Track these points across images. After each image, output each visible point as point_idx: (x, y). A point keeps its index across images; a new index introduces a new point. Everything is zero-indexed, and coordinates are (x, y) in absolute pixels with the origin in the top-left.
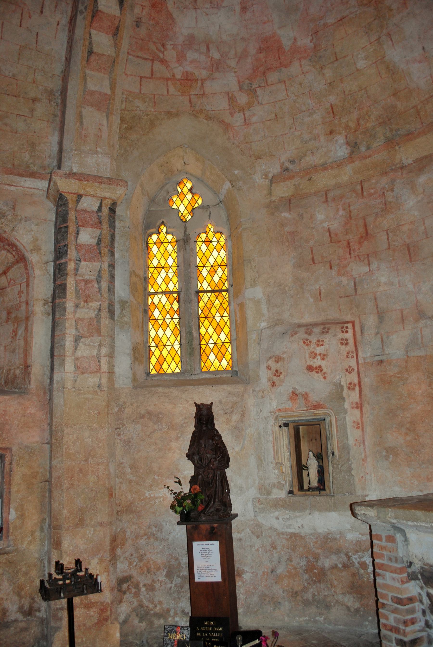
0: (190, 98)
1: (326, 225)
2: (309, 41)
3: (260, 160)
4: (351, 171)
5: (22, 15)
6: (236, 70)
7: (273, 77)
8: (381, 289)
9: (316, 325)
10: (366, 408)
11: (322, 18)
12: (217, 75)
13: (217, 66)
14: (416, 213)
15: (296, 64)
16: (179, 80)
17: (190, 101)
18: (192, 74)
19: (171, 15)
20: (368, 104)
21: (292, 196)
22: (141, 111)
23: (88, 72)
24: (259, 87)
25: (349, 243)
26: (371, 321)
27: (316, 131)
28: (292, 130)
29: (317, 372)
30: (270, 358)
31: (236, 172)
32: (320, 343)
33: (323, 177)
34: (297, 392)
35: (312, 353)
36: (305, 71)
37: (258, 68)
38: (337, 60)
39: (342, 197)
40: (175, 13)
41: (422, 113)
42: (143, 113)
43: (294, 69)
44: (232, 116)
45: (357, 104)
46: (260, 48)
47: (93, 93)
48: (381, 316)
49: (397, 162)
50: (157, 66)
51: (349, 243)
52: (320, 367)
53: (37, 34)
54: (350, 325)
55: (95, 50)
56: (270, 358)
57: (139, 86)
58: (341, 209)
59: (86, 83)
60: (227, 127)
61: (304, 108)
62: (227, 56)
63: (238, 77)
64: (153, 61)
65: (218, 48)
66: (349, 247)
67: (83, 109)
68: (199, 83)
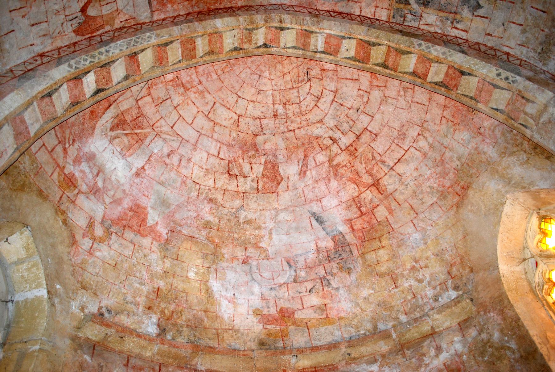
0: (62, 195)
2: (165, 233)
4: (156, 351)
5: (21, 8)
6: (106, 207)
7: (129, 235)
11: (180, 226)
12: (92, 197)
13: (96, 191)
16: (65, 174)
17: (61, 197)
19: (94, 129)
20: (184, 306)
22: (24, 168)
23: (35, 103)
24: (116, 233)
27: (138, 299)
28: (121, 285)
31: (58, 286)
33: (133, 342)
36: (153, 249)
37: (122, 219)
38: (177, 259)
40: (98, 131)
41: (221, 337)
42: (24, 171)
43: (146, 242)
44: (83, 238)
45: (177, 301)
46: (131, 208)
47: (23, 121)
49: (193, 363)
50: (59, 149)
53: (13, 31)
55: (54, 96)
57: (37, 149)
59: (26, 109)
60: (74, 243)
61: (138, 275)
63: (105, 212)
64: (60, 142)
65: (104, 180)
67: (7, 124)
68: (76, 191)
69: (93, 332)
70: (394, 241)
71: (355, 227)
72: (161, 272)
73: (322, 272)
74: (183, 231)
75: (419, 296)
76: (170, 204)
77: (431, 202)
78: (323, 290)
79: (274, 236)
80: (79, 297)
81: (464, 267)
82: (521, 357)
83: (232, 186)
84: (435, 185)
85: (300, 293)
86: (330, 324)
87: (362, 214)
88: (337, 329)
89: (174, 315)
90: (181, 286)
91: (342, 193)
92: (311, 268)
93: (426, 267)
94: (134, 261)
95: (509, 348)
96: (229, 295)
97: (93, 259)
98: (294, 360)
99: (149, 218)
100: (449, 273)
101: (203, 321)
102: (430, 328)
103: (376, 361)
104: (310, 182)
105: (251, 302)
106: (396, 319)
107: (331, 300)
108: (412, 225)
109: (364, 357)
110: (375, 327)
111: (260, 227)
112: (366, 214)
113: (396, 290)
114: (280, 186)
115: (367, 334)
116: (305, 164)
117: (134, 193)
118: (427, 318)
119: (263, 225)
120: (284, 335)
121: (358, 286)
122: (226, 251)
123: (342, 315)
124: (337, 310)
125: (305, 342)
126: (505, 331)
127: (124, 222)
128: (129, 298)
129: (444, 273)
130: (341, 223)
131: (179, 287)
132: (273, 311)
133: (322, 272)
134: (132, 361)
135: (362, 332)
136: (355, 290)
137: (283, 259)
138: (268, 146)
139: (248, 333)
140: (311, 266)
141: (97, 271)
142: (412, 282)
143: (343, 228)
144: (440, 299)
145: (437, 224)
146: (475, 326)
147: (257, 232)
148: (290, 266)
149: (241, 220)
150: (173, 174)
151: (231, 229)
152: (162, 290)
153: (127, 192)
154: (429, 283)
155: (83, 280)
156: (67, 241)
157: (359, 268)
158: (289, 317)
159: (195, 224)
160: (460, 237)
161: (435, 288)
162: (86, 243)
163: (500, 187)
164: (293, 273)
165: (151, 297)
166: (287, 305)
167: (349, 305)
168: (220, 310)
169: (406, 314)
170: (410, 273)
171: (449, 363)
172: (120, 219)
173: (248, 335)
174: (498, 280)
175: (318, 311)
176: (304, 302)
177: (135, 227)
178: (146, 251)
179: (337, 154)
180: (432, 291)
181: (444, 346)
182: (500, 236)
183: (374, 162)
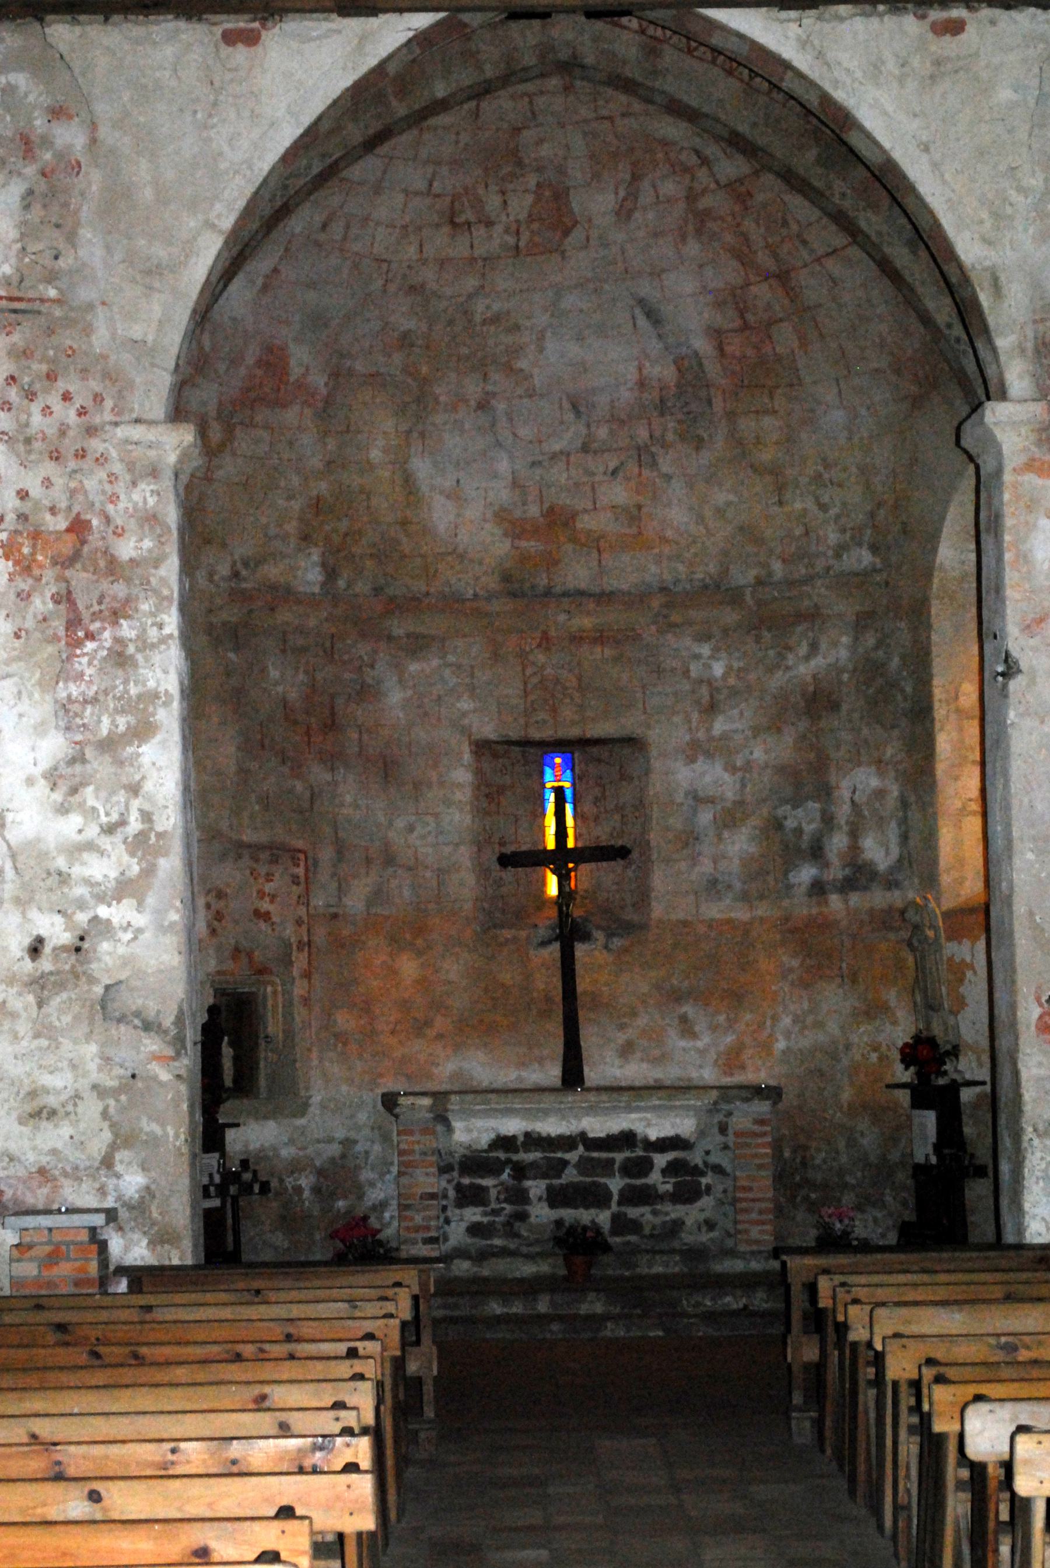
10: (316, 977)
12: (199, 380)
14: (401, 715)
15: (296, 408)
24: (241, 423)
26: (326, 854)
30: (209, 892)
43: (291, 415)
48: (341, 850)
52: (268, 913)
54: (302, 856)
56: (209, 892)
69: (231, 615)
71: (729, 349)
73: (642, 434)
75: (813, 535)
78: (640, 474)
83: (460, 249)
87: (746, 327)
90: (357, 481)
91: (709, 272)
92: (622, 422)
93: (840, 485)
95: (902, 691)
98: (562, 617)
99: (293, 362)
100: (872, 515)
101: (398, 542)
104: (641, 234)
105: (491, 494)
106: (765, 565)
111: (517, 327)
114: (570, 239)
115: (707, 580)
116: (633, 195)
120: (551, 562)
122: (442, 391)
123: (669, 533)
132: (534, 511)
133: (643, 434)
138: (545, 151)
140: (623, 416)
142: (810, 504)
143: (701, 344)
144: (845, 557)
147: (509, 339)
148: (578, 413)
149: (478, 318)
150: (334, 260)
154: (838, 517)
161: (843, 531)
164: (584, 431)
166: (565, 500)
169: (784, 561)
179: (704, 191)
181: (823, 646)
183: (784, 232)
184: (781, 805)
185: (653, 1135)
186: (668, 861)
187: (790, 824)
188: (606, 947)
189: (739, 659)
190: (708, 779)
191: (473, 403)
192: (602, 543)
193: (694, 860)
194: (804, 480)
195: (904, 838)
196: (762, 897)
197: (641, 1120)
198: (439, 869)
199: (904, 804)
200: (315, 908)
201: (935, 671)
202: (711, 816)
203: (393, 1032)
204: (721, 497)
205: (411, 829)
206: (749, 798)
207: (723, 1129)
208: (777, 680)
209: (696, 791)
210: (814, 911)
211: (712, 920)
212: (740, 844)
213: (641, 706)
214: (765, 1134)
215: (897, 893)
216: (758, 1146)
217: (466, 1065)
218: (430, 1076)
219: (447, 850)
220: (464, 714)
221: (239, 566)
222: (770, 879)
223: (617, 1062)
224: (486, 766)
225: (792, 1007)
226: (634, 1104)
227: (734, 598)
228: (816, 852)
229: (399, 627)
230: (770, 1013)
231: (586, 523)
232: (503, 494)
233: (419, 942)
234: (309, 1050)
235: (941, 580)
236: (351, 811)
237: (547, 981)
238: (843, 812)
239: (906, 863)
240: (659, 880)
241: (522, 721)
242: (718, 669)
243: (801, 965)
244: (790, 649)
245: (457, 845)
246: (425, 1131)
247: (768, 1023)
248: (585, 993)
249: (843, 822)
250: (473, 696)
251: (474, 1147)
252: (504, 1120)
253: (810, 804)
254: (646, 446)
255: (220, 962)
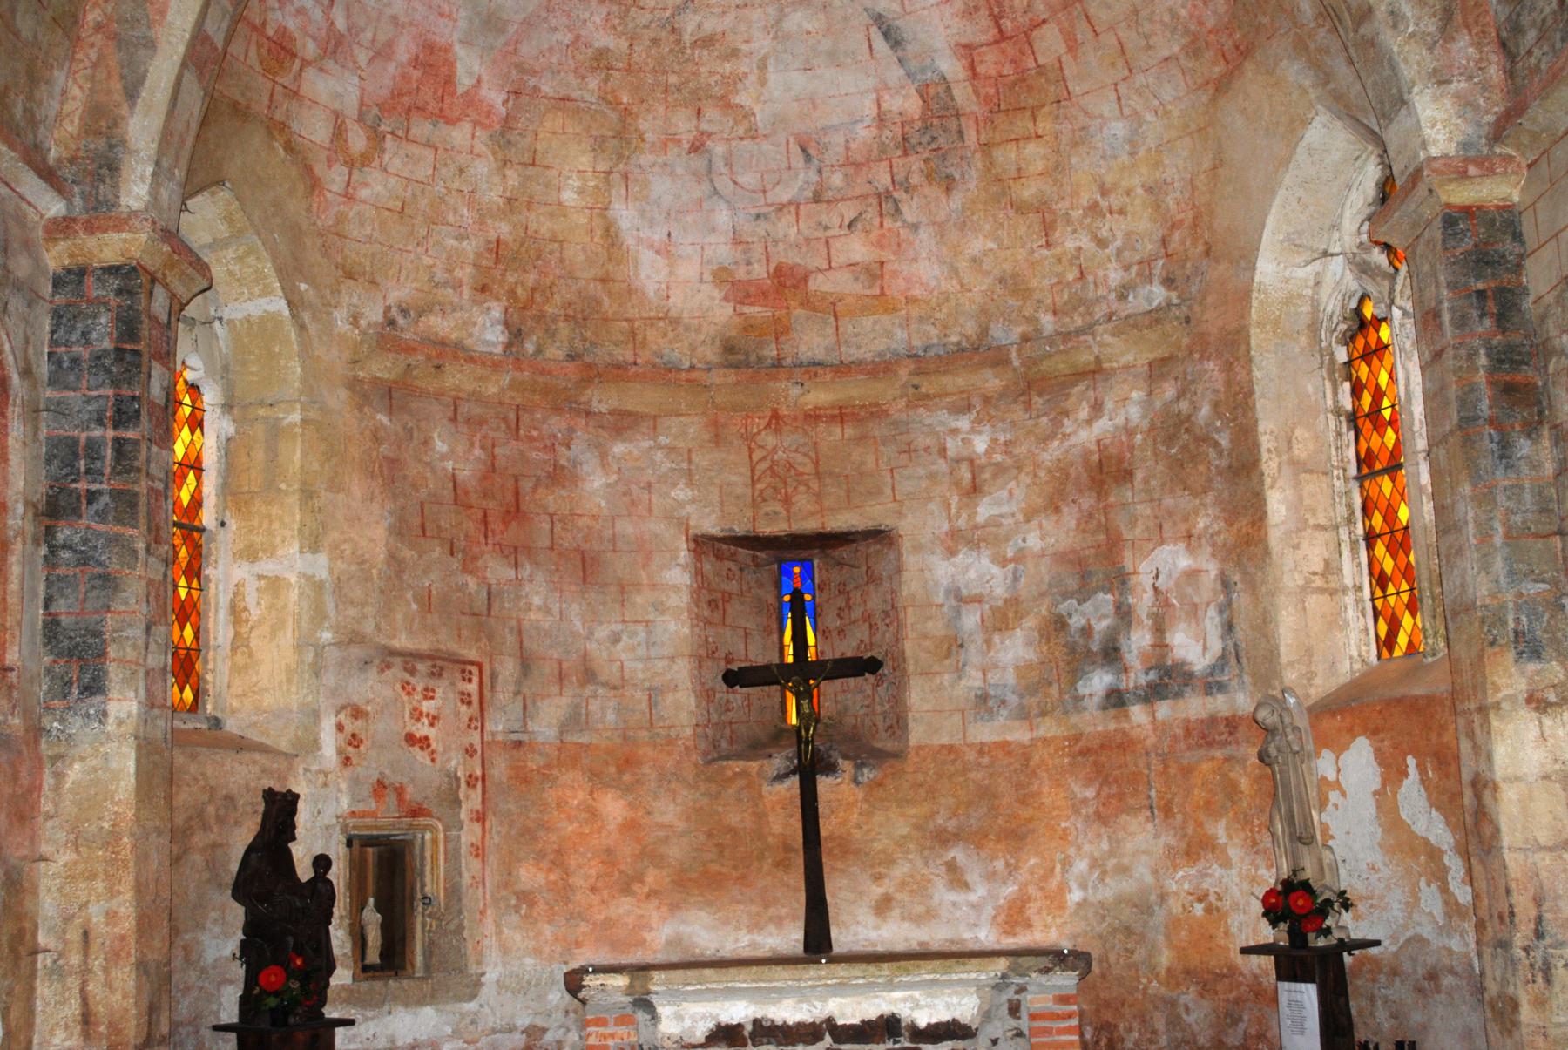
1: (449, 465)
2: (500, 101)
3: (351, 282)
7: (421, 128)
8: (533, 616)
9: (418, 656)
10: (491, 821)
11: (534, 73)
12: (330, 64)
14: (603, 504)
18: (292, 39)
20: (558, 272)
21: (396, 382)
24: (392, 133)
25: (485, 515)
26: (508, 668)
27: (458, 273)
28: (419, 249)
29: (422, 748)
30: (343, 708)
31: (303, 286)
32: (428, 694)
34: (387, 782)
35: (415, 709)
36: (476, 151)
37: (401, 95)
38: (533, 164)
39: (482, 422)
41: (640, 338)
43: (460, 135)
44: (330, 166)
48: (526, 664)
51: (485, 515)
52: (426, 738)
54: (475, 670)
56: (343, 708)
58: (477, 445)
60: (314, 185)
61: (451, 218)
62: (357, 34)
63: (363, 90)
66: (486, 524)
69: (383, 368)
70: (1066, 127)
71: (981, 69)
72: (501, 201)
73: (884, 180)
74: (543, 88)
75: (1090, 278)
76: (506, 23)
77: (1167, 53)
78: (882, 225)
79: (772, 76)
80: (345, 298)
81: (1195, 241)
82: (1230, 467)
84: (1183, 12)
85: (826, 228)
86: (886, 311)
87: (1002, 37)
88: (901, 325)
89: (537, 296)
90: (545, 227)
92: (858, 165)
93: (1122, 212)
94: (440, 188)
95: (1216, 444)
96: (657, 237)
97: (356, 208)
98: (795, 391)
99: (460, 70)
100: (1164, 242)
101: (599, 303)
102: (1092, 358)
103: (969, 408)
105: (708, 252)
107: (895, 253)
108: (1113, 97)
109: (947, 395)
110: (984, 332)
111: (735, 53)
112: (1011, 38)
113: (1045, 252)
117: (418, 17)
118: (1089, 338)
119: (744, 47)
120: (780, 330)
121: (962, 227)
122: (649, 125)
123: (917, 292)
124: (908, 280)
125: (826, 348)
126: (1222, 409)
127: (406, 100)
128: (440, 276)
129: (1155, 237)
130: (948, 51)
131: (543, 230)
132: (759, 271)
133: (884, 180)
134: (464, 408)
135: (954, 339)
136: (954, 235)
137: (792, 140)
139: (700, 325)
140: (859, 159)
141: (368, 230)
142: (1085, 241)
143: (950, 66)
144: (1131, 298)
145: (1167, 113)
146: (1176, 379)
147: (728, 68)
148: (808, 158)
149: (687, 38)
151: (660, 64)
152: (506, 244)
153: (402, 19)
154: (1119, 252)
155: (345, 258)
156: (301, 187)
157: (972, 181)
158: (795, 287)
159: (571, 62)
160: (1206, 165)
161: (1127, 268)
162: (335, 178)
163: (1307, 83)
164: (814, 178)
165: (484, 263)
166: (793, 258)
167: (937, 270)
168: (637, 275)
169: (1055, 313)
170: (1085, 216)
171: (1107, 442)
172: (397, 94)
173: (698, 330)
174: (1245, 296)
175: (862, 277)
176: (833, 252)
177: (433, 106)
178: (462, 159)
180: (1121, 273)
181: (1109, 405)
182: (1282, 192)
184: (1065, 599)
185: (922, 1023)
186: (926, 673)
187: (1076, 622)
188: (855, 781)
189: (1004, 431)
190: (972, 574)
191: (686, 146)
192: (840, 307)
193: (959, 671)
194: (1076, 214)
195: (1229, 627)
196: (1043, 714)
197: (905, 1000)
198: (649, 689)
199: (1226, 584)
200: (493, 734)
201: (1260, 414)
202: (978, 617)
203: (593, 889)
204: (977, 244)
205: (615, 639)
206: (1024, 594)
207: (1014, 1010)
208: (1052, 453)
209: (959, 589)
210: (1112, 726)
211: (982, 744)
212: (1016, 649)
213: (888, 491)
214: (1070, 1016)
215: (1220, 698)
216: (1061, 1031)
217: (685, 929)
218: (642, 943)
219: (660, 664)
220: (681, 504)
221: (394, 311)
222: (1054, 690)
223: (871, 920)
224: (707, 567)
225: (1087, 848)
226: (896, 980)
227: (998, 359)
228: (1111, 654)
229: (602, 400)
230: (1059, 856)
231: (818, 284)
232: (723, 251)
233: (626, 777)
234: (482, 913)
235: (1261, 302)
236: (539, 616)
237: (786, 824)
238: (1143, 603)
239: (1233, 661)
240: (918, 697)
241: (749, 513)
242: (980, 445)
243: (1098, 793)
244: (1066, 413)
245: (672, 659)
246: (623, 1020)
247: (1058, 869)
248: (831, 838)
249: (1144, 617)
250: (690, 484)
251: (687, 1040)
252: (727, 1004)
253: (1101, 595)
254: (887, 191)
255: (355, 799)
